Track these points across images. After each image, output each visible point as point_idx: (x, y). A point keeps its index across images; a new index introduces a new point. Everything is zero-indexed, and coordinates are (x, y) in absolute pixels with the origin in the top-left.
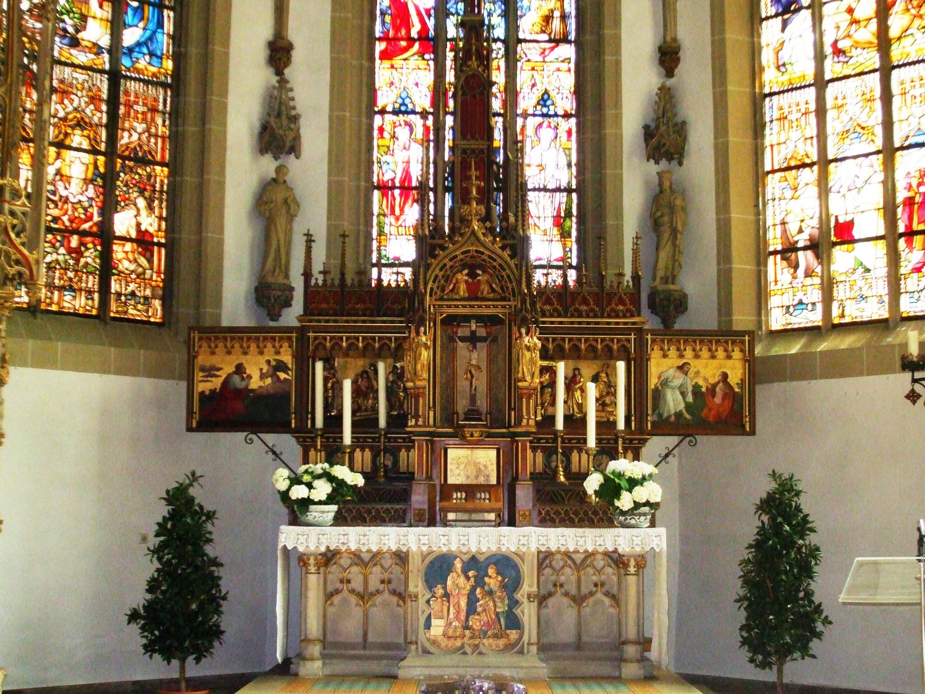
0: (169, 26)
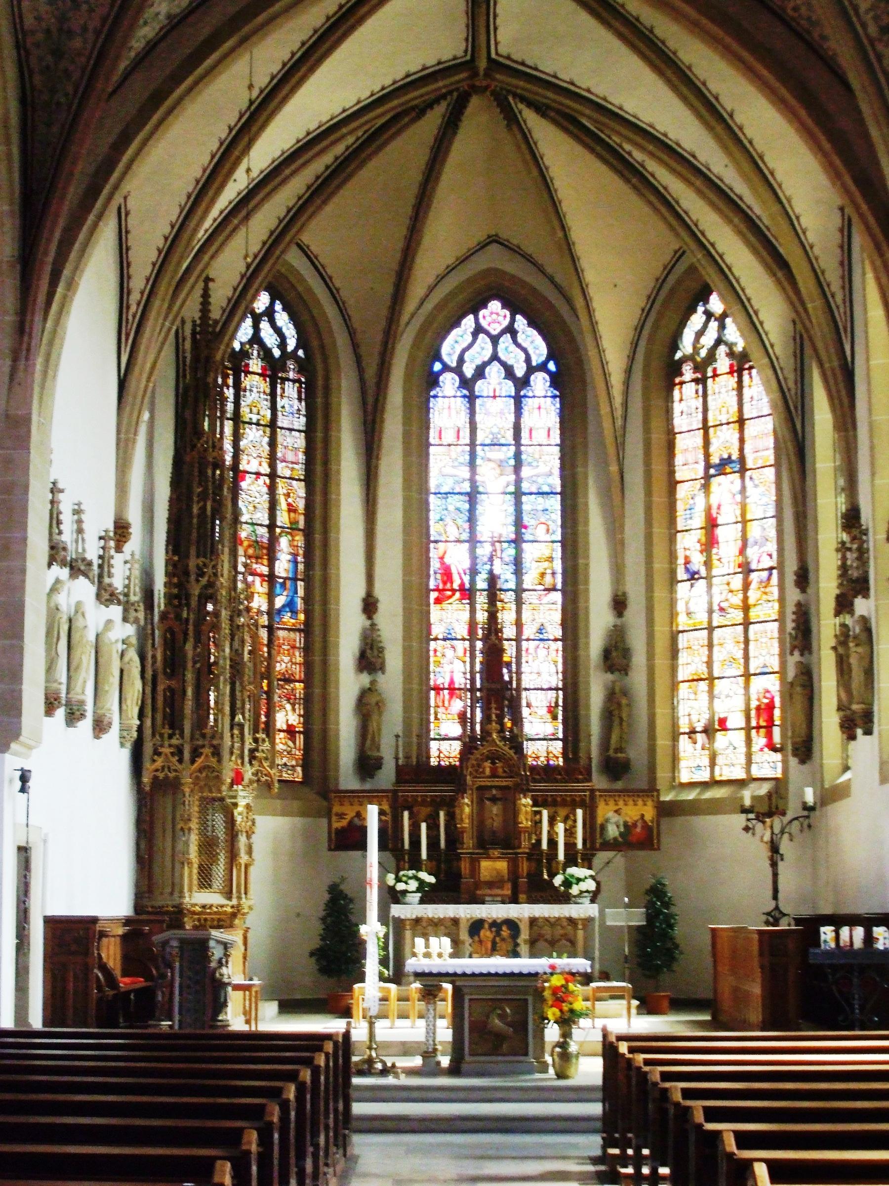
0: (301, 592)
